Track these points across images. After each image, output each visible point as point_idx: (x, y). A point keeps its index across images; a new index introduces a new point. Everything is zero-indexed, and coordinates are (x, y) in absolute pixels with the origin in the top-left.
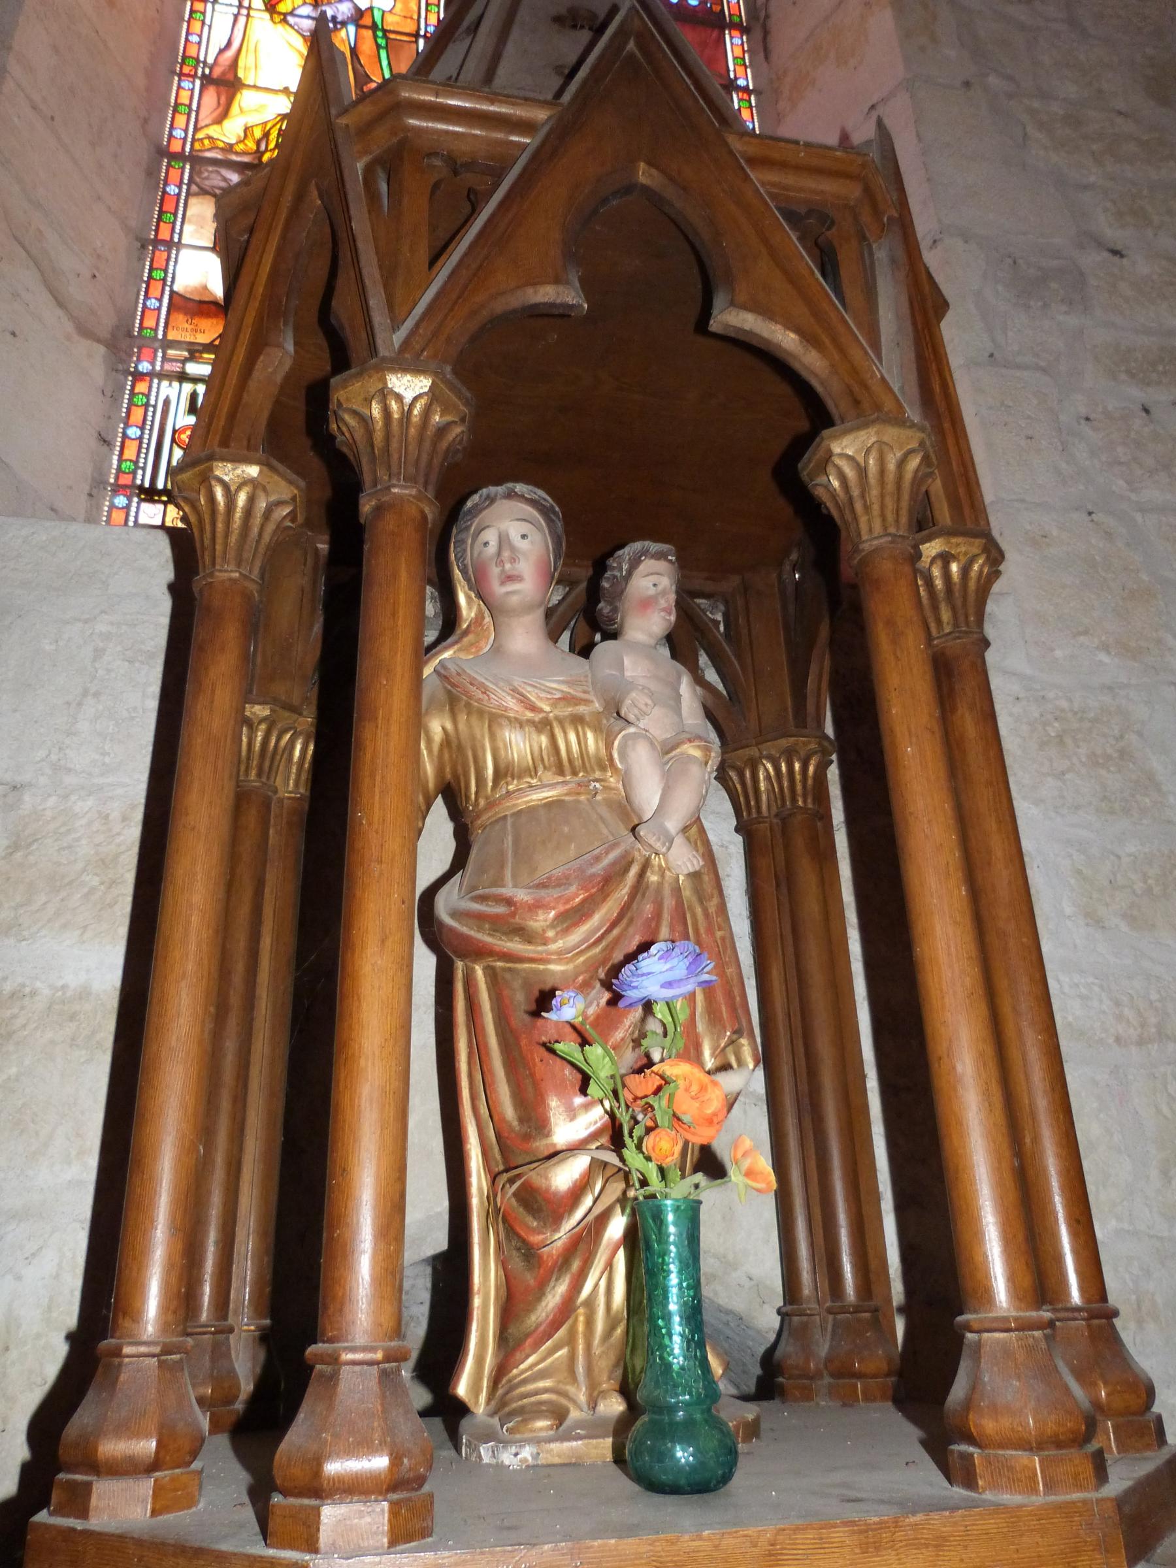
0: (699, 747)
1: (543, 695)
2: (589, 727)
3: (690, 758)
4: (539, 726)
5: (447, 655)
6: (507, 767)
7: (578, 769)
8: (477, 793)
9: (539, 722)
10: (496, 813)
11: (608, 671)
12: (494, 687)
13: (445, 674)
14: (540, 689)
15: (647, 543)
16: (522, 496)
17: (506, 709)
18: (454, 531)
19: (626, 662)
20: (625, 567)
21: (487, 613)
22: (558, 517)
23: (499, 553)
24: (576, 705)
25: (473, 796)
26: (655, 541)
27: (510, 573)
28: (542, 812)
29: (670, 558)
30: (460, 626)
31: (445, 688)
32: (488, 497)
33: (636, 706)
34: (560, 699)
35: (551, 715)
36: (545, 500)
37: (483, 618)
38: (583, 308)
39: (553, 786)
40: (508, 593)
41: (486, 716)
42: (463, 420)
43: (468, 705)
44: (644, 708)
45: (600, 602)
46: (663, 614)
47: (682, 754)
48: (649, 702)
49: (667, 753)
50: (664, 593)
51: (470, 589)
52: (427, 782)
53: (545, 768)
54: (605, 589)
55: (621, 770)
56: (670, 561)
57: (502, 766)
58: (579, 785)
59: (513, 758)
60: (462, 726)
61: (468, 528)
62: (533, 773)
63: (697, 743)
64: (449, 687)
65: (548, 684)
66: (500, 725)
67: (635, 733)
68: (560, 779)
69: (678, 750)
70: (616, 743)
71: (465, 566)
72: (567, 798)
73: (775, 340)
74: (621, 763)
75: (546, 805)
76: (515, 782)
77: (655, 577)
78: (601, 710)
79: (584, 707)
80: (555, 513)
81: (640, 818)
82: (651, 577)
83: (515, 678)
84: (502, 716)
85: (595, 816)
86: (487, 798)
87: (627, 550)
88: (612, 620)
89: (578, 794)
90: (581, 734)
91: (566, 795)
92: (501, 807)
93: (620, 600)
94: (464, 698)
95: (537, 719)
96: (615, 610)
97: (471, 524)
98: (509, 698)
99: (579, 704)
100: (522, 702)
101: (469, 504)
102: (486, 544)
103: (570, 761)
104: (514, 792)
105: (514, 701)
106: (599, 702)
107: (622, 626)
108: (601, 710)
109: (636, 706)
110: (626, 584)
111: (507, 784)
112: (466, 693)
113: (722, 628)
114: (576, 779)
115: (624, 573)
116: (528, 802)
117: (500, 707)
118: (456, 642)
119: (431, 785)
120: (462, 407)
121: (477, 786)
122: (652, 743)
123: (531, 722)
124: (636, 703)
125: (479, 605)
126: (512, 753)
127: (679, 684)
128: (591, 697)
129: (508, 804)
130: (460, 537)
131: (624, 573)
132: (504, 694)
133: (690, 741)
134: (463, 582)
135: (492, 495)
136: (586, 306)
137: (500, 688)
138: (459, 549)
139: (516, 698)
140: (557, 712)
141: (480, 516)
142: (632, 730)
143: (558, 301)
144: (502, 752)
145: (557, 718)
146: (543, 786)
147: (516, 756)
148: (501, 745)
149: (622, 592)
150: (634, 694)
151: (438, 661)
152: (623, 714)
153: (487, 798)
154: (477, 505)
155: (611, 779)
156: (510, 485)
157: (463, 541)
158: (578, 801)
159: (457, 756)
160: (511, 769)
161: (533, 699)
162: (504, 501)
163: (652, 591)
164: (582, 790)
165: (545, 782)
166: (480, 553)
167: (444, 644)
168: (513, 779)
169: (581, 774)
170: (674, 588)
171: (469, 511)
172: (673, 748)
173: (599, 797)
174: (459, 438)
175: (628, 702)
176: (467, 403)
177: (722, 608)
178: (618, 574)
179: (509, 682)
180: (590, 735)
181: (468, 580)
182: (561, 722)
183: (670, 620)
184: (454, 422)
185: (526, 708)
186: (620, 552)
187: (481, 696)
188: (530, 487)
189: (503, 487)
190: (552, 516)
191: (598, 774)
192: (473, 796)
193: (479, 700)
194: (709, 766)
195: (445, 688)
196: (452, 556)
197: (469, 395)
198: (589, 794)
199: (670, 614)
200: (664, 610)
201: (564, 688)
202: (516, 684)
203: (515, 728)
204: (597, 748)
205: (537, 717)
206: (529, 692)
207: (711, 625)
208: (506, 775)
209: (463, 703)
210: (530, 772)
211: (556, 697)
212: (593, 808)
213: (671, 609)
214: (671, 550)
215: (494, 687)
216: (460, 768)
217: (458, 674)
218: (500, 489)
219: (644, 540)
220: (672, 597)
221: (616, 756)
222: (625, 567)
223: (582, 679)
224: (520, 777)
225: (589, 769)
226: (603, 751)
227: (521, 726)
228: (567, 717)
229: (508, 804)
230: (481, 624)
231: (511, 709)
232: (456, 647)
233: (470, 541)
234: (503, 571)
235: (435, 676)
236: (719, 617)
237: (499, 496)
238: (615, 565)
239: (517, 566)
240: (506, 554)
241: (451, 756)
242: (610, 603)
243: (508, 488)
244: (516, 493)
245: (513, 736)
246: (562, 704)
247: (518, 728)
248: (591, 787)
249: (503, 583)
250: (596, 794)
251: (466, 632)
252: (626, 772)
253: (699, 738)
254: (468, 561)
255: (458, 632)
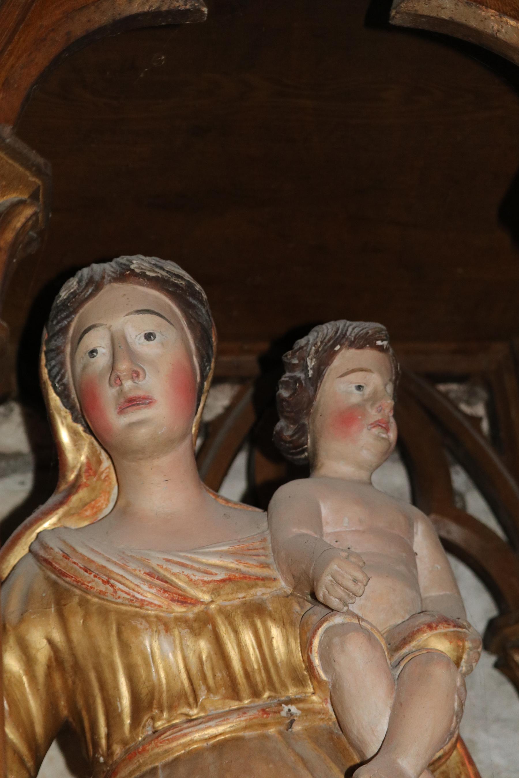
0: (445, 635)
1: (198, 577)
2: (274, 620)
3: (431, 653)
4: (195, 625)
5: (47, 524)
6: (152, 693)
7: (260, 687)
8: (109, 736)
9: (196, 620)
10: (140, 766)
11: (295, 530)
12: (121, 572)
13: (47, 556)
14: (192, 568)
15: (341, 324)
16: (143, 275)
17: (142, 604)
18: (45, 336)
19: (325, 511)
20: (311, 363)
21: (104, 456)
22: (201, 301)
23: (113, 367)
24: (251, 587)
25: (103, 742)
26: (352, 318)
27: (132, 395)
28: (209, 758)
29: (379, 343)
30: (65, 476)
31: (48, 578)
32: (91, 281)
33: (339, 584)
34: (223, 581)
35: (213, 606)
36: (178, 276)
37: (99, 462)
38: (202, 12)
39: (223, 716)
40: (131, 425)
41: (113, 617)
42: (34, 196)
43: (83, 603)
44: (350, 585)
45: (278, 420)
46: (376, 431)
47: (420, 649)
48: (359, 576)
49: (397, 649)
50: (374, 398)
51: (76, 420)
52: (32, 724)
53: (209, 689)
54: (284, 400)
55: (326, 683)
56: (381, 349)
57: (144, 691)
58: (264, 711)
59: (159, 678)
60: (76, 636)
61: (64, 330)
62: (191, 700)
63: (442, 629)
64: (53, 576)
65: (204, 559)
66: (135, 630)
67: (343, 624)
68: (235, 705)
69: (414, 644)
70: (316, 642)
71: (65, 387)
72: (248, 734)
73: (489, 31)
74: (326, 672)
75: (214, 747)
76: (165, 715)
77: (361, 374)
78: (289, 590)
79: (264, 590)
80: (195, 294)
81: (361, 753)
82: (352, 377)
83: (153, 554)
84: (136, 615)
85: (292, 758)
86: (125, 743)
87: (311, 337)
88: (300, 447)
89: (264, 725)
90: (261, 631)
91: (245, 728)
92: (147, 755)
93: (308, 414)
94: (78, 592)
95: (191, 615)
96: (302, 430)
97: (69, 323)
98: (145, 587)
99: (256, 586)
100: (165, 591)
101: (64, 294)
102: (93, 353)
103: (247, 675)
104: (165, 731)
105: (154, 591)
106: (286, 580)
107: (315, 454)
108: (289, 590)
109: (339, 584)
110: (316, 390)
111: (153, 718)
112: (79, 584)
113: (485, 426)
114: (259, 702)
115: (311, 373)
116: (189, 744)
117: (132, 601)
118: (61, 503)
119: (39, 729)
120: (32, 179)
121: (108, 725)
122: (370, 637)
123: (182, 621)
124: (339, 578)
125: (92, 444)
126: (157, 672)
127: (411, 535)
128: (273, 572)
129: (156, 750)
130: (54, 344)
131: (311, 373)
132: (137, 582)
133: (430, 627)
134: (65, 412)
135: (97, 278)
136: (205, 10)
137: (131, 573)
138: (53, 363)
139: (156, 586)
140: (220, 602)
141: (81, 311)
142: (338, 620)
143: (165, 8)
144: (142, 671)
145: (221, 611)
146: (209, 718)
147: (162, 675)
148: (139, 660)
149: (311, 401)
150: (334, 567)
151: (34, 535)
152: (320, 596)
153: (125, 743)
154: (74, 294)
155: (315, 698)
156: (123, 259)
157: (59, 351)
158: (266, 737)
159: (74, 683)
160: (156, 694)
161: (181, 584)
162: (115, 285)
163: (356, 397)
164: (270, 719)
165: (211, 710)
166: (85, 367)
167: (42, 508)
168: (162, 711)
169: (266, 695)
170: (390, 388)
171: (64, 304)
172: (405, 642)
173: (297, 728)
174: (30, 222)
175: (327, 579)
176: (38, 172)
177: (483, 394)
178: (302, 376)
179: (143, 562)
180: (275, 632)
181: (71, 408)
182: (228, 617)
183: (387, 440)
184: (21, 203)
185: (173, 600)
186: (302, 342)
187: (102, 587)
188: (153, 260)
189: (113, 263)
190: (191, 299)
191: (292, 692)
192: (103, 742)
193: (101, 595)
194: (463, 663)
195: (47, 578)
196: (45, 372)
197: (40, 160)
198: (280, 723)
199: (387, 430)
200: (377, 424)
201: (230, 563)
202: (154, 563)
203: (158, 632)
204: (289, 651)
205: (191, 613)
206: (175, 574)
207: (467, 424)
208: (150, 706)
209: (76, 600)
210: (187, 698)
211: (219, 578)
212: (289, 745)
213: (388, 422)
214: (380, 331)
215: (121, 572)
216: (81, 703)
217: (66, 556)
218: (109, 267)
219: (336, 319)
220: (389, 403)
221: (317, 662)
222: (311, 363)
223: (257, 545)
224: (171, 708)
225: (278, 685)
226: (298, 655)
227: (167, 630)
228: (237, 607)
229: (156, 750)
230: (95, 473)
231: (150, 603)
232: (61, 511)
233: (68, 349)
234: (121, 392)
235: (31, 560)
236: (480, 410)
237: (107, 278)
238: (296, 361)
239: (141, 382)
240: (123, 366)
241: (65, 682)
242: (294, 421)
243: (120, 264)
244: (133, 270)
245: (156, 645)
246: (228, 588)
247: (163, 633)
248: (283, 714)
249: (122, 411)
250: (292, 722)
251: (75, 487)
252: (334, 686)
253: (446, 621)
254: (69, 378)
255: (63, 487)
